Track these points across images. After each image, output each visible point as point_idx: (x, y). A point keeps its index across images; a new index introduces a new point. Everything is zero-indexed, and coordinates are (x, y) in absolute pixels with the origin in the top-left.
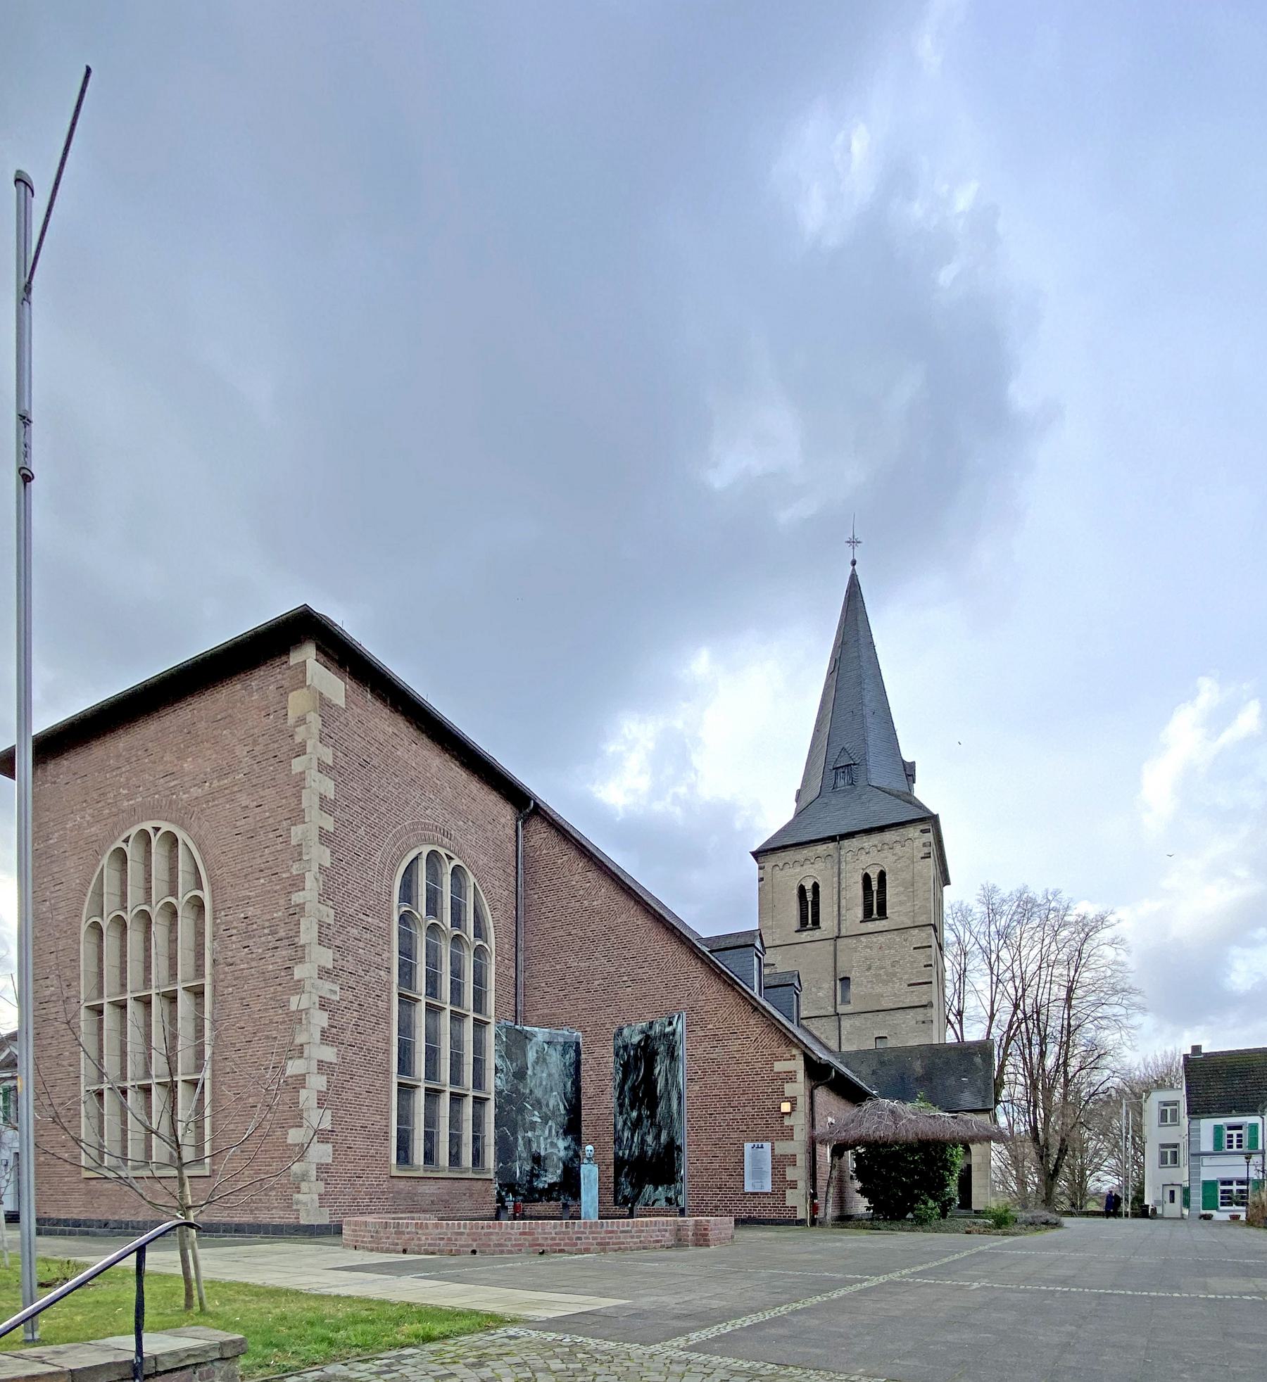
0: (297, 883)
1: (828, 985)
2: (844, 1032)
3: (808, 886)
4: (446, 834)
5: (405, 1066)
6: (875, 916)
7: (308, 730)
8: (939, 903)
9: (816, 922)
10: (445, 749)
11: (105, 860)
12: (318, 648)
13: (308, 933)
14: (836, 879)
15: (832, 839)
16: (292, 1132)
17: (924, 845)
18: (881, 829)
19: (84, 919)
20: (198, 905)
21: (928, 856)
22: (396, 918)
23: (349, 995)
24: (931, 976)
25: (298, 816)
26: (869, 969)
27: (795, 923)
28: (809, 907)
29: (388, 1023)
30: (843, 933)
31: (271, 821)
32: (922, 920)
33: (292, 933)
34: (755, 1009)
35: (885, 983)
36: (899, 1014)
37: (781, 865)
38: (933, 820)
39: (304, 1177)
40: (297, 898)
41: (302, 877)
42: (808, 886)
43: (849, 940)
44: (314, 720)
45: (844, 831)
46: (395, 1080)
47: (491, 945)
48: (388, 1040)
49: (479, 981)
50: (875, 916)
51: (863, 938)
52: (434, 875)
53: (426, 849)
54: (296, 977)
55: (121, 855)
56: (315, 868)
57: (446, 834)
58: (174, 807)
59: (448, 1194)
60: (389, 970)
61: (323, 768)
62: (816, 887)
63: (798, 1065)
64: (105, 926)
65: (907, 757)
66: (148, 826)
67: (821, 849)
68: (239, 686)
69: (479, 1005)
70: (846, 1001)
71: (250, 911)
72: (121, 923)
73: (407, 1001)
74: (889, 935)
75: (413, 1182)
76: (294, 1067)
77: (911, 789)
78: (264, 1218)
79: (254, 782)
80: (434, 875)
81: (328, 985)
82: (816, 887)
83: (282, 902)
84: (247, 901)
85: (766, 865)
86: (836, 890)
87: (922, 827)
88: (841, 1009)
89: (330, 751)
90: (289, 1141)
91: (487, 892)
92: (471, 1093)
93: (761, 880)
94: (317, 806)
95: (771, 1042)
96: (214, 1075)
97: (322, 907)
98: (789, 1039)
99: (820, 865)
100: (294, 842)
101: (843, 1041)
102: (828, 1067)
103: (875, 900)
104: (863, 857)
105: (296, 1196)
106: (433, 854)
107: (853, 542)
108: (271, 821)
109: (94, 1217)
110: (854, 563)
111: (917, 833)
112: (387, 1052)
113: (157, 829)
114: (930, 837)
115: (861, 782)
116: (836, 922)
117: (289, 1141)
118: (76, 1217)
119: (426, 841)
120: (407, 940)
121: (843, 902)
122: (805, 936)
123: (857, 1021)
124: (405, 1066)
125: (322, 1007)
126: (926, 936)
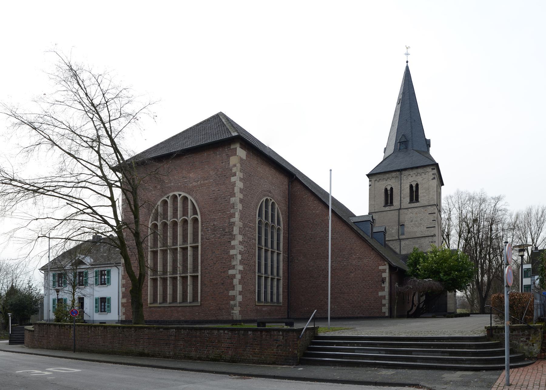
2: (402, 246)
3: (389, 188)
4: (270, 192)
6: (414, 201)
8: (439, 194)
11: (159, 203)
12: (241, 144)
13: (236, 230)
14: (399, 186)
15: (398, 170)
16: (231, 292)
17: (433, 174)
18: (417, 168)
19: (150, 221)
20: (195, 220)
21: (434, 178)
22: (257, 222)
25: (233, 195)
27: (383, 203)
30: (402, 207)
32: (432, 203)
34: (373, 249)
38: (437, 165)
39: (235, 305)
40: (232, 220)
41: (234, 214)
42: (389, 188)
43: (404, 210)
44: (238, 165)
45: (403, 168)
48: (255, 262)
49: (278, 240)
50: (414, 201)
51: (410, 210)
52: (267, 207)
53: (265, 199)
55: (165, 202)
57: (270, 192)
61: (241, 180)
62: (392, 189)
63: (387, 267)
65: (427, 137)
66: (177, 193)
67: (394, 174)
68: (212, 153)
70: (403, 234)
71: (215, 223)
72: (165, 225)
73: (260, 249)
74: (420, 209)
76: (231, 272)
77: (428, 150)
78: (220, 318)
80: (267, 207)
82: (392, 189)
83: (227, 221)
84: (214, 220)
85: (372, 180)
87: (432, 167)
88: (401, 237)
89: (242, 174)
90: (230, 294)
91: (280, 209)
98: (383, 259)
99: (393, 180)
103: (414, 194)
104: (410, 178)
105: (232, 311)
106: (267, 200)
107: (407, 54)
110: (407, 62)
111: (430, 170)
112: (255, 266)
113: (180, 195)
114: (435, 171)
115: (410, 147)
117: (230, 294)
119: (265, 196)
120: (260, 228)
122: (387, 208)
123: (407, 242)
124: (259, 271)
125: (240, 254)
126: (434, 209)
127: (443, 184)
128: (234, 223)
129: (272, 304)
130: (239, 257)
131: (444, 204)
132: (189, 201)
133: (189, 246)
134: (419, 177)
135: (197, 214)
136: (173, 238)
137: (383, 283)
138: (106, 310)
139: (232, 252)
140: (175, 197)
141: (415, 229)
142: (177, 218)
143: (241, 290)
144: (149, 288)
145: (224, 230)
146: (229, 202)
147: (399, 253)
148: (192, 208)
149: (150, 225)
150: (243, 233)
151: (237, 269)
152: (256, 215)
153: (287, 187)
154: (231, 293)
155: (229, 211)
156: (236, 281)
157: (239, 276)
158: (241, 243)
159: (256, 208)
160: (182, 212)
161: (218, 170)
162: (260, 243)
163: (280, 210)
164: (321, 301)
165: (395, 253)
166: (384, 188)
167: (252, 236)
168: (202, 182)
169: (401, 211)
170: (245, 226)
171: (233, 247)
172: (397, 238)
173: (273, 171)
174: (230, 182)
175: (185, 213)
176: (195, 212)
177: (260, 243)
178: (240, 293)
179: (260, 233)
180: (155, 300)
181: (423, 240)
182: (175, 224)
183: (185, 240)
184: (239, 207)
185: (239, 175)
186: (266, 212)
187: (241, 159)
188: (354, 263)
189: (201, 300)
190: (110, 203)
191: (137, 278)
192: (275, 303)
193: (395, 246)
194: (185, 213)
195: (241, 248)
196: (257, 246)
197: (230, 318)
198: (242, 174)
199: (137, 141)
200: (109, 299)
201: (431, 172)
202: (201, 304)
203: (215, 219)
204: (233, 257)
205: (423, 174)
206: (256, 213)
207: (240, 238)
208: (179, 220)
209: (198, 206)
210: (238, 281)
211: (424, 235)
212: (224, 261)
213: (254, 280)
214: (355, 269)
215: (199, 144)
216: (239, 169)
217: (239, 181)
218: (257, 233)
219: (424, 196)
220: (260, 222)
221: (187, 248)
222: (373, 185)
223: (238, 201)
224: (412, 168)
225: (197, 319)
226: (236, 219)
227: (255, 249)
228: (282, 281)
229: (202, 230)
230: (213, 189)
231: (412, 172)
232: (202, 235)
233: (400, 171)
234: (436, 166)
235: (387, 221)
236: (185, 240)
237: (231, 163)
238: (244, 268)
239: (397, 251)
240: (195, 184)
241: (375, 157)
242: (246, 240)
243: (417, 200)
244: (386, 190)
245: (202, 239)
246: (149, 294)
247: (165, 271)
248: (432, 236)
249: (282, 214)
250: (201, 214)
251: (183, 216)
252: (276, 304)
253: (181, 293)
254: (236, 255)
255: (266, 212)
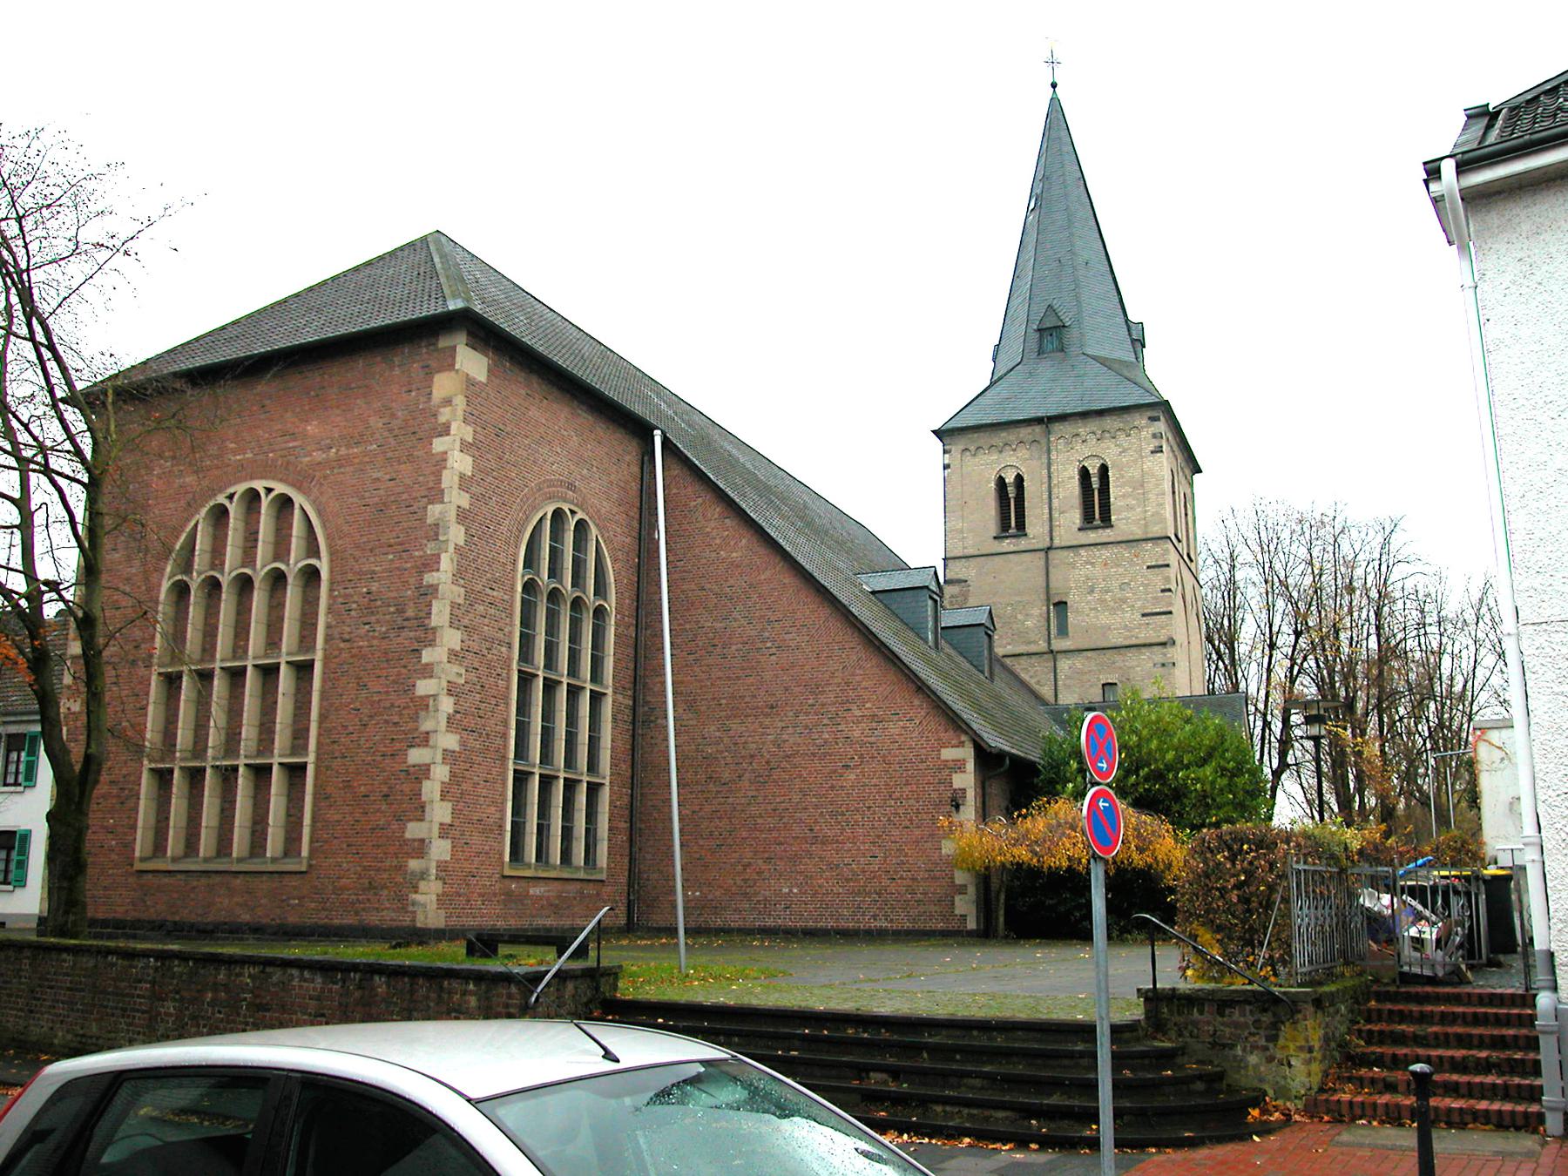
0: (432, 564)
1: (1038, 610)
2: (1061, 676)
3: (1010, 478)
4: (571, 487)
5: (521, 751)
6: (1097, 522)
7: (454, 412)
8: (1185, 505)
9: (1021, 526)
10: (574, 397)
12: (469, 333)
13: (440, 614)
15: (1039, 421)
16: (410, 825)
18: (1100, 413)
20: (311, 575)
21: (1159, 450)
22: (520, 589)
23: (473, 676)
24: (1171, 604)
25: (436, 495)
26: (1092, 591)
27: (993, 527)
28: (1011, 504)
29: (507, 704)
30: (1057, 542)
31: (405, 496)
32: (1156, 531)
33: (422, 614)
35: (1113, 611)
36: (1130, 653)
37: (972, 448)
38: (1165, 406)
39: (423, 875)
40: (429, 578)
42: (1010, 478)
43: (1065, 553)
44: (460, 402)
46: (511, 767)
47: (611, 604)
48: (506, 723)
50: (1097, 522)
51: (1082, 552)
52: (556, 535)
53: (550, 510)
54: (424, 661)
55: (221, 514)
56: (451, 548)
57: (571, 487)
58: (291, 468)
59: (559, 897)
60: (510, 645)
61: (465, 447)
62: (1019, 480)
63: (967, 753)
64: (194, 587)
66: (260, 485)
67: (1024, 432)
69: (596, 676)
70: (1063, 631)
71: (375, 587)
75: (523, 883)
76: (416, 756)
77: (1139, 358)
78: (373, 919)
79: (390, 455)
80: (556, 535)
81: (456, 669)
82: (1019, 480)
83: (412, 581)
86: (1045, 487)
87: (1150, 414)
88: (1058, 644)
89: (470, 429)
90: (408, 835)
91: (608, 541)
92: (585, 778)
93: (946, 467)
94: (456, 486)
95: (934, 724)
96: (318, 758)
97: (455, 588)
99: (1023, 452)
100: (429, 521)
101: (1060, 688)
102: (1001, 755)
103: (1095, 498)
106: (558, 515)
108: (405, 496)
109: (144, 916)
110: (1054, 86)
112: (505, 736)
113: (269, 490)
114: (1161, 426)
115: (1073, 350)
116: (1047, 528)
117: (408, 835)
118: (118, 916)
119: (550, 498)
121: (1055, 503)
122: (1007, 545)
123: (1078, 662)
124: (521, 751)
125: (450, 693)
127: (1197, 470)
128: (434, 588)
129: (565, 875)
130: (447, 705)
131: (1208, 531)
132: (297, 512)
133: (283, 660)
134: (1110, 443)
135: (317, 555)
136: (237, 635)
137: (957, 807)
138: (11, 877)
139: (424, 687)
140: (253, 497)
141: (1104, 619)
142: (254, 567)
143: (448, 820)
144: (142, 803)
145: (401, 611)
146: (422, 520)
147: (1052, 700)
148: (303, 534)
149: (166, 585)
150: (466, 622)
151: (439, 746)
152: (514, 562)
153: (636, 469)
154: (413, 830)
155: (422, 547)
156: (430, 791)
157: (441, 772)
158: (454, 655)
159: (518, 538)
160: (270, 548)
161: (393, 416)
162: (526, 654)
163: (608, 544)
164: (746, 866)
165: (1044, 703)
166: (993, 477)
167: (500, 635)
168: (343, 451)
169: (1052, 554)
170: (473, 597)
171: (428, 671)
172: (1043, 646)
173: (585, 418)
174: (430, 454)
175: (281, 549)
176: (312, 549)
177: (526, 654)
178: (445, 830)
179: (527, 621)
180: (159, 847)
181: (1132, 658)
182: (244, 584)
183: (273, 640)
184: (456, 534)
185: (461, 431)
186: (555, 554)
187: (470, 382)
188: (857, 734)
189: (312, 851)
190: (14, 517)
191: (77, 768)
192: (578, 868)
193: (1035, 674)
194: (281, 549)
195: (455, 672)
196: (515, 666)
197: (406, 921)
198: (470, 429)
199: (123, 321)
200: (26, 837)
201: (1148, 430)
202: (310, 866)
203: (374, 572)
204: (425, 704)
205: (1122, 437)
206: (516, 555)
207: (451, 639)
208: (260, 572)
209: (324, 526)
210: (437, 788)
211: (1134, 641)
212: (396, 719)
213: (498, 786)
214: (861, 756)
215: (342, 331)
216: (460, 413)
217: (456, 453)
218: (518, 622)
219: (1130, 508)
220: (530, 587)
221: (276, 667)
222: (955, 464)
223: (452, 515)
224: (1085, 415)
225: (292, 919)
226: (444, 574)
227: (508, 679)
228: (607, 789)
229: (330, 610)
230: (375, 475)
231: (1083, 429)
232: (328, 626)
233: (1046, 421)
234: (1163, 409)
235: (1006, 591)
236: (273, 640)
237: (438, 393)
238: (463, 743)
239: (1046, 691)
240: (319, 456)
241: (962, 371)
242: (475, 647)
243: (1106, 520)
244: (1001, 482)
245: (328, 638)
246: (140, 824)
247: (199, 748)
248: (1163, 644)
249: (615, 561)
250: (333, 553)
251: (275, 559)
252: (582, 875)
253: (249, 824)
254: (435, 697)
255: (555, 554)
